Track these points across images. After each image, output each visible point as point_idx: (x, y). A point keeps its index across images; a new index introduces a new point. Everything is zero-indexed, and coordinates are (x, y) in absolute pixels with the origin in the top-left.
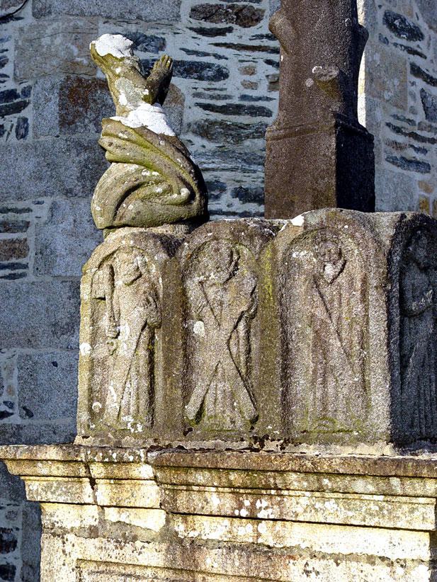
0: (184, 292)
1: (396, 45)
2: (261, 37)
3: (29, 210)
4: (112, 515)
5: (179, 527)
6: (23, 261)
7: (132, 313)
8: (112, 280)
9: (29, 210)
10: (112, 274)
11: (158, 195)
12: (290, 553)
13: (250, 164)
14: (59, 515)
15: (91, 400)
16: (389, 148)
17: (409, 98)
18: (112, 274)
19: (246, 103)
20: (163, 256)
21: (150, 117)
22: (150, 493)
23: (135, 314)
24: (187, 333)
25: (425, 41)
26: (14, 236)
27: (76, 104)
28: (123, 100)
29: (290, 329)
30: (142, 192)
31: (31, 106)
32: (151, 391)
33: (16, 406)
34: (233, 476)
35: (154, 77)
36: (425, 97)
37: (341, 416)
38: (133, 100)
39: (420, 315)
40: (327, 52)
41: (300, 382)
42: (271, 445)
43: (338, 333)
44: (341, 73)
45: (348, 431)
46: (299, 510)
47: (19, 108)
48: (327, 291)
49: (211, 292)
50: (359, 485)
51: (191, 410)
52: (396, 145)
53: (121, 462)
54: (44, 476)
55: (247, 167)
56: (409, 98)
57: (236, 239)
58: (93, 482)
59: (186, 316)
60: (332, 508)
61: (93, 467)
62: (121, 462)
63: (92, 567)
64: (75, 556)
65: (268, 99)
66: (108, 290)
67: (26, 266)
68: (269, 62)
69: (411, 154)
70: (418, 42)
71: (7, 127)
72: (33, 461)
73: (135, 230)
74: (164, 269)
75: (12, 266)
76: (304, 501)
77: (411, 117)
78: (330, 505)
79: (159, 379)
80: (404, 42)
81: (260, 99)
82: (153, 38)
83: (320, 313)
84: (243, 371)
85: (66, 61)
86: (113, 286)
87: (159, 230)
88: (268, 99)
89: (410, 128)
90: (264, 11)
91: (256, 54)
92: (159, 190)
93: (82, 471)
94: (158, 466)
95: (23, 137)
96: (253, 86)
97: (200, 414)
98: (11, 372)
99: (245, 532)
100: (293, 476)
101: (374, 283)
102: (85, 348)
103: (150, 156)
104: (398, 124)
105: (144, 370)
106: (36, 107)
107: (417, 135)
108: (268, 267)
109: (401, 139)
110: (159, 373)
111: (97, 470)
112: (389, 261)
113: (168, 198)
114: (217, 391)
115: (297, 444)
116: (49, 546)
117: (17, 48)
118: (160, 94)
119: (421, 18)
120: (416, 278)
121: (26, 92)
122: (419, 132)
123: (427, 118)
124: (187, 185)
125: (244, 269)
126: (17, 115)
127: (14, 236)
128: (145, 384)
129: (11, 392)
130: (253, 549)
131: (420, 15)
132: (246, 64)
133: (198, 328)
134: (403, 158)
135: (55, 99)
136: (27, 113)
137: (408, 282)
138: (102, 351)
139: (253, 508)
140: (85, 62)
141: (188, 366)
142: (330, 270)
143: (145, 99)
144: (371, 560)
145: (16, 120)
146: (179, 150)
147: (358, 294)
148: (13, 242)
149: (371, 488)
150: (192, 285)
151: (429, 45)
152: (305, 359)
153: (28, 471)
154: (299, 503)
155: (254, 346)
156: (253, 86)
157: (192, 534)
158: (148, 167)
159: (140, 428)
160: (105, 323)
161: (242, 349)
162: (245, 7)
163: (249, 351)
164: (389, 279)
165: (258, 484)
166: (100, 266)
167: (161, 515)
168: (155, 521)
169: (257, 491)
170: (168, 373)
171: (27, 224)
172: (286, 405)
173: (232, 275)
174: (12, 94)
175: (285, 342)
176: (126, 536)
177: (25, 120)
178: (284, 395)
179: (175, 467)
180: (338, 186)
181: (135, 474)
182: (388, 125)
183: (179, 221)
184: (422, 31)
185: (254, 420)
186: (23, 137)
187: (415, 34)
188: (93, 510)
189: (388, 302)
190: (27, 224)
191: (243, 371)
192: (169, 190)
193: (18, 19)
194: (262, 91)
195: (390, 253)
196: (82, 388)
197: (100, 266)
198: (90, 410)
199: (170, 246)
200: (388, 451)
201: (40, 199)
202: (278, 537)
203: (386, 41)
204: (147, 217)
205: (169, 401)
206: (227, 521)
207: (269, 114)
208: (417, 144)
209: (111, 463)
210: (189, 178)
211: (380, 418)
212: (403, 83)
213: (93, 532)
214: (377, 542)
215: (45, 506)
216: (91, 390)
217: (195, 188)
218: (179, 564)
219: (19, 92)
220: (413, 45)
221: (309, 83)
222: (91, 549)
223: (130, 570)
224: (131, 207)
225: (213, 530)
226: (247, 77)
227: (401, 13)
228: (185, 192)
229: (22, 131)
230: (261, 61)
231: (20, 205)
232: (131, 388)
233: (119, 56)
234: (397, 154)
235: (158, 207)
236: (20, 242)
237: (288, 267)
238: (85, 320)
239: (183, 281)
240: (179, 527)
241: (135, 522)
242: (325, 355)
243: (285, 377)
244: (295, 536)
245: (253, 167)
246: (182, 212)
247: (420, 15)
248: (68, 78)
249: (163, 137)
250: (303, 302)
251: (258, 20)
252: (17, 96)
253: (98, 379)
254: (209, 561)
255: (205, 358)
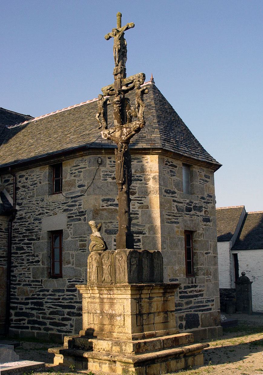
0: (102, 261)
1: (168, 196)
2: (136, 197)
3: (86, 237)
4: (92, 295)
5: (101, 296)
6: (85, 248)
7: (95, 265)
8: (92, 259)
9: (86, 237)
10: (92, 258)
11: (98, 246)
12: (115, 299)
13: (134, 225)
14: (85, 295)
15: (89, 278)
16: (166, 220)
17: (172, 208)
18: (92, 258)
19: (133, 212)
20: (99, 256)
21: (97, 234)
22: (97, 291)
23: (95, 265)
24: (102, 267)
25: (177, 194)
26: (84, 243)
27: (96, 214)
28: (93, 231)
29: (116, 267)
30: (96, 246)
31: (87, 214)
32: (98, 276)
33: (85, 280)
34: (107, 288)
35: (98, 228)
36: (177, 207)
37: (122, 279)
38: (95, 231)
39: (134, 265)
40: (125, 223)
41: (117, 275)
42: (113, 284)
43: (122, 268)
44: (127, 226)
45: (123, 282)
46: (115, 292)
47: (84, 215)
48: (120, 262)
49: (105, 261)
50: (122, 289)
51: (103, 279)
52: (169, 219)
53: (93, 287)
54: (82, 289)
55: (133, 226)
56: (172, 208)
57: (109, 254)
58: (89, 290)
59: (102, 265)
60: (119, 292)
61: (89, 288)
62: (93, 287)
63: (90, 303)
64: (87, 301)
65: (138, 211)
66: (91, 261)
67: (86, 249)
68: (138, 203)
69: (173, 220)
70: (175, 194)
71: (82, 219)
72: (81, 287)
73: (95, 252)
74: (99, 258)
75: (83, 249)
76: (116, 291)
77: (173, 212)
78: (119, 292)
79: (99, 275)
80: (171, 195)
81: (136, 211)
82: (112, 199)
83: (119, 265)
84: (110, 273)
85: (94, 205)
86: (92, 260)
87: (99, 252)
88: (138, 211)
89: (173, 214)
90: (136, 192)
91: (135, 201)
92: (99, 245)
93: (88, 289)
94: (98, 287)
95: (85, 221)
96: (134, 208)
97: (104, 280)
98: (84, 272)
99: (109, 296)
100: (114, 288)
101: (126, 261)
102: (88, 270)
103: (97, 240)
104: (170, 214)
105: (97, 273)
106: (88, 215)
107: (175, 215)
108: (113, 258)
109: (170, 217)
110: (99, 273)
111: (90, 288)
112: (128, 257)
113: (100, 246)
114: (106, 276)
115: (116, 284)
116: (83, 300)
117: (84, 202)
118: (99, 230)
119: (175, 189)
120: (133, 259)
121: (86, 211)
122: (175, 215)
123: (178, 211)
124: (103, 245)
125: (110, 258)
126: (84, 216)
127: (84, 243)
128: (97, 275)
129: (83, 277)
130: (110, 298)
131: (175, 188)
132: (133, 204)
133: (104, 267)
134: (171, 222)
135: (91, 213)
136: (86, 216)
137: (131, 260)
138: (91, 271)
139: (110, 293)
140: (98, 205)
141: (103, 273)
142: (120, 259)
143: (97, 231)
144: (124, 299)
145: (83, 217)
146: (102, 239)
147: (124, 262)
148: (83, 244)
149: (123, 289)
150: (103, 260)
151: (178, 194)
152: (118, 272)
153: (80, 289)
154: (115, 292)
155: (111, 269)
156: (134, 208)
157: (103, 297)
158: (97, 242)
159: (96, 282)
160: (91, 266)
161: (110, 270)
162: (132, 191)
163: (111, 270)
164: (128, 260)
165: (110, 289)
166: (90, 257)
167: (99, 294)
168: (98, 295)
169: (110, 290)
170: (100, 274)
171: (86, 240)
172: (115, 278)
173: (108, 259)
174: (83, 212)
175: (115, 269)
176: (94, 298)
177: (85, 218)
178: (115, 277)
179: (99, 287)
180: (126, 244)
181: (94, 289)
182: (167, 215)
183: (102, 250)
184: (176, 191)
185: (111, 280)
186: (85, 221)
187: (174, 193)
188: (90, 294)
189: (128, 263)
190: (86, 240)
191: (110, 273)
192: (100, 245)
193: (84, 196)
194: (136, 209)
195: (128, 256)
196: (88, 276)
197: (90, 257)
198: (89, 279)
199: (100, 254)
200: (127, 284)
201: (89, 235)
202: (113, 297)
203: (165, 196)
204: (97, 250)
205: (100, 278)
206: (107, 295)
207: (138, 214)
208: (175, 218)
209: (91, 287)
210: (103, 244)
211: (127, 280)
212: (171, 205)
213: (90, 298)
214: (124, 296)
215: (83, 294)
216: (89, 276)
217: (104, 244)
218: (101, 301)
219: (84, 211)
220: (173, 195)
221: (122, 228)
222: (89, 300)
223: (95, 303)
224: (94, 248)
225: (105, 296)
226: (133, 206)
227: (170, 189)
228: (103, 246)
229: (85, 220)
230: (136, 203)
231: (85, 236)
232: (95, 276)
233: (93, 224)
234: (169, 221)
235: (99, 248)
236: (85, 244)
237: (115, 258)
238: (88, 266)
239: (102, 260)
240: (101, 296)
241: (95, 296)
242: (120, 271)
243: (115, 274)
244: (115, 296)
245: (135, 226)
246: (102, 249)
247: (175, 188)
248: (94, 209)
249: (99, 237)
250: (117, 264)
251: (135, 194)
252: (84, 212)
253: (90, 275)
254: (105, 301)
255: (105, 271)
